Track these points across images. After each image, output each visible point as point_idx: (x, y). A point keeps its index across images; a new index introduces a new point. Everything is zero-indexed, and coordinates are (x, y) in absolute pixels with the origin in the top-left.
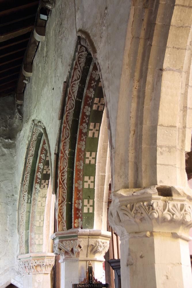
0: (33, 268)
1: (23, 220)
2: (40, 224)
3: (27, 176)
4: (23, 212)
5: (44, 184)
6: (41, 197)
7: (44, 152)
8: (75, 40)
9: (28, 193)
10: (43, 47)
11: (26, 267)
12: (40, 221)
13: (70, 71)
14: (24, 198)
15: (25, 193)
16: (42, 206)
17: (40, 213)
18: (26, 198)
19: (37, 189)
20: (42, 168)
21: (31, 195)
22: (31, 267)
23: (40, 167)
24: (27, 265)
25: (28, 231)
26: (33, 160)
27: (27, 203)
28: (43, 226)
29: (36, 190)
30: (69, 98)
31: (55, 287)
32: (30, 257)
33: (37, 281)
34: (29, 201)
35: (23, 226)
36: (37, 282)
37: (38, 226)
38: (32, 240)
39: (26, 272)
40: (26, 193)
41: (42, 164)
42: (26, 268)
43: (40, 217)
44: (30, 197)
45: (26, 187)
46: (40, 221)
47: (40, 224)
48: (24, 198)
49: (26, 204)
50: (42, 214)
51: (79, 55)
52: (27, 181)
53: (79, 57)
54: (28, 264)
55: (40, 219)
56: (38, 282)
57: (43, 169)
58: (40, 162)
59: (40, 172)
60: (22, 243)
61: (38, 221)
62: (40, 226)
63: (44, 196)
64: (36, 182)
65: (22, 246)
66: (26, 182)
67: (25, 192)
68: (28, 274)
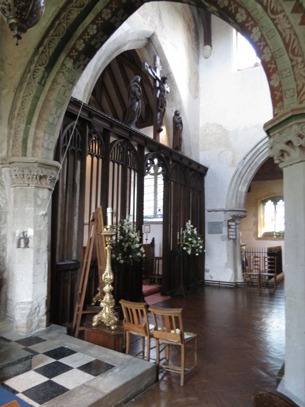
0: (36, 178)
1: (23, 107)
2: (54, 121)
3: (53, 39)
4: (27, 96)
5: (80, 63)
6: (68, 81)
7: (114, 6)
8: (170, 20)
9: (46, 69)
10: (145, 389)
11: (25, 176)
12: (55, 116)
13: (143, 117)
14: (34, 75)
15: (39, 67)
16: (64, 95)
17: (58, 104)
18: (39, 75)
19: (66, 67)
20: (91, 33)
21: (48, 74)
22: (35, 177)
23: (89, 31)
24: (26, 172)
25: (29, 126)
26: (79, 15)
27: (40, 83)
28: (56, 125)
29: (64, 67)
30: (60, 23)
31: (1, 321)
32: (36, 162)
33: (41, 196)
34: (43, 83)
35: (22, 117)
36: (39, 198)
37: (50, 123)
38: (37, 140)
39: (23, 182)
40: (42, 69)
41: (95, 27)
42: (23, 177)
43: (57, 110)
44: (46, 75)
45: (46, 59)
46: (55, 116)
47: (54, 121)
48: (34, 75)
49: (37, 84)
50: (61, 107)
51: (35, 68)
52: (49, 48)
53: (35, 71)
54: (31, 172)
55: (56, 114)
56: (42, 198)
57: (94, 36)
58: (93, 23)
59: (84, 40)
60: (15, 141)
61: (53, 115)
62: (52, 124)
63: (72, 81)
64: (69, 56)
65: (15, 145)
66: (65, 20)
67: (40, 65)
68: (27, 185)
